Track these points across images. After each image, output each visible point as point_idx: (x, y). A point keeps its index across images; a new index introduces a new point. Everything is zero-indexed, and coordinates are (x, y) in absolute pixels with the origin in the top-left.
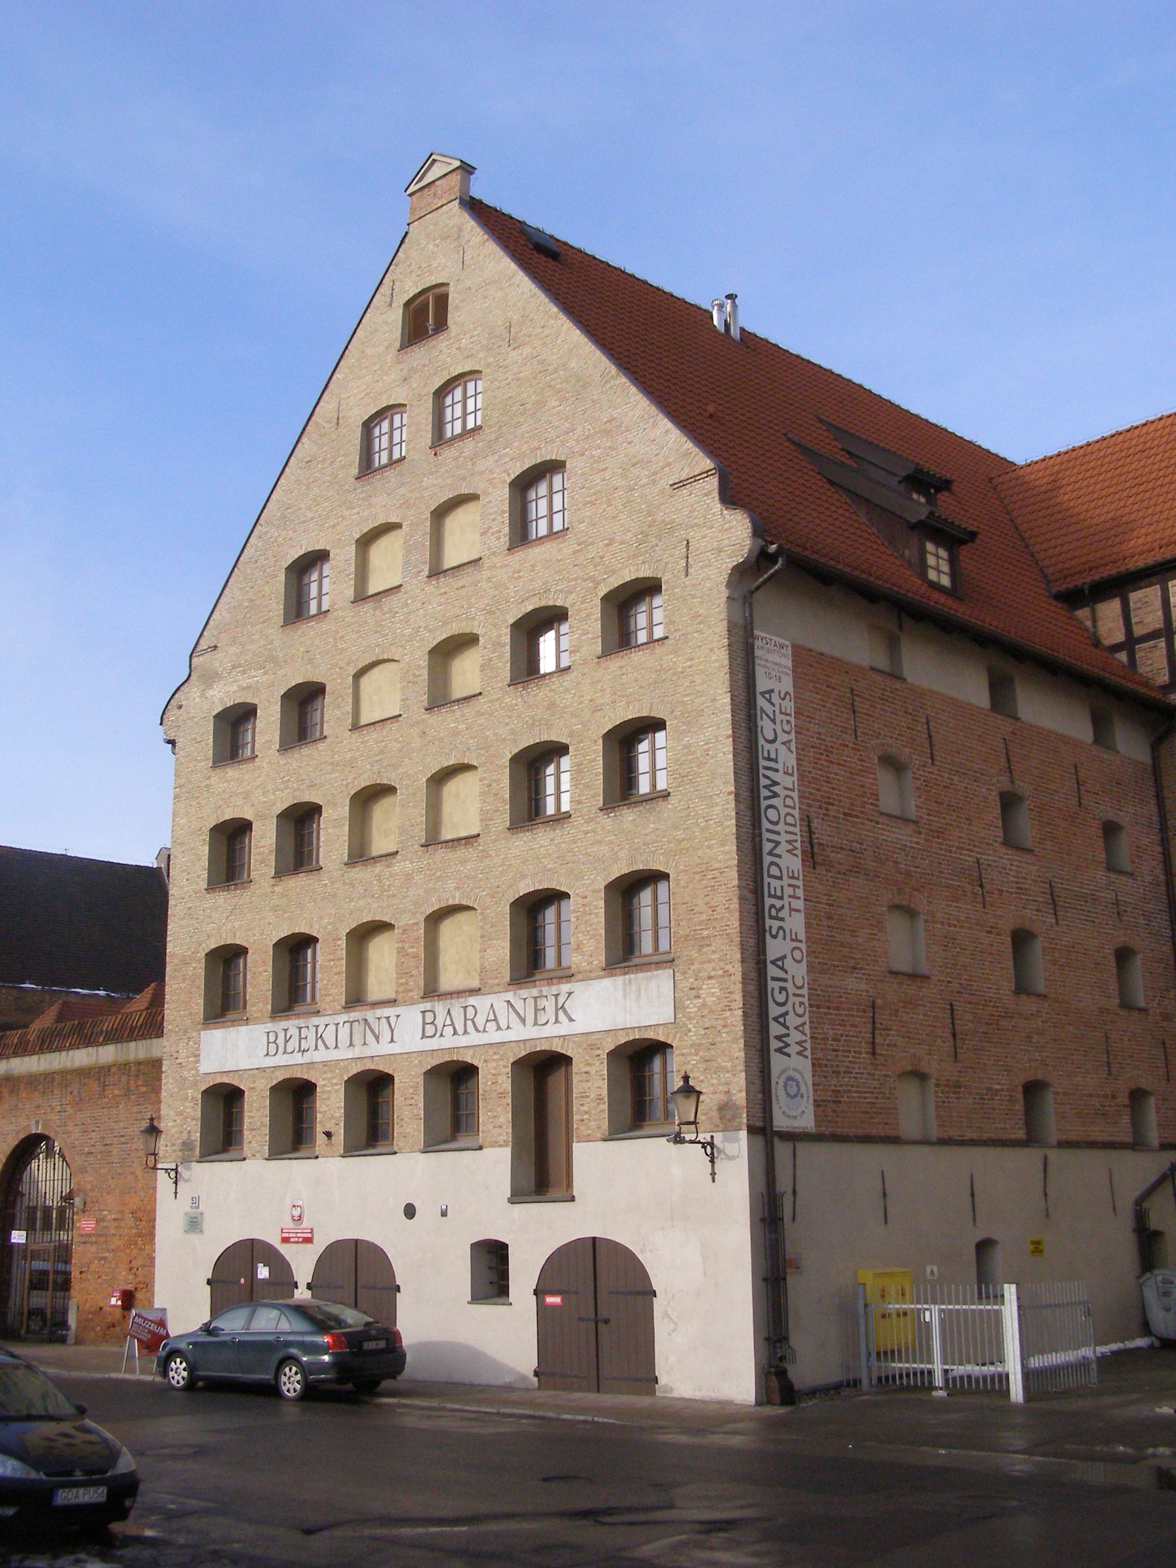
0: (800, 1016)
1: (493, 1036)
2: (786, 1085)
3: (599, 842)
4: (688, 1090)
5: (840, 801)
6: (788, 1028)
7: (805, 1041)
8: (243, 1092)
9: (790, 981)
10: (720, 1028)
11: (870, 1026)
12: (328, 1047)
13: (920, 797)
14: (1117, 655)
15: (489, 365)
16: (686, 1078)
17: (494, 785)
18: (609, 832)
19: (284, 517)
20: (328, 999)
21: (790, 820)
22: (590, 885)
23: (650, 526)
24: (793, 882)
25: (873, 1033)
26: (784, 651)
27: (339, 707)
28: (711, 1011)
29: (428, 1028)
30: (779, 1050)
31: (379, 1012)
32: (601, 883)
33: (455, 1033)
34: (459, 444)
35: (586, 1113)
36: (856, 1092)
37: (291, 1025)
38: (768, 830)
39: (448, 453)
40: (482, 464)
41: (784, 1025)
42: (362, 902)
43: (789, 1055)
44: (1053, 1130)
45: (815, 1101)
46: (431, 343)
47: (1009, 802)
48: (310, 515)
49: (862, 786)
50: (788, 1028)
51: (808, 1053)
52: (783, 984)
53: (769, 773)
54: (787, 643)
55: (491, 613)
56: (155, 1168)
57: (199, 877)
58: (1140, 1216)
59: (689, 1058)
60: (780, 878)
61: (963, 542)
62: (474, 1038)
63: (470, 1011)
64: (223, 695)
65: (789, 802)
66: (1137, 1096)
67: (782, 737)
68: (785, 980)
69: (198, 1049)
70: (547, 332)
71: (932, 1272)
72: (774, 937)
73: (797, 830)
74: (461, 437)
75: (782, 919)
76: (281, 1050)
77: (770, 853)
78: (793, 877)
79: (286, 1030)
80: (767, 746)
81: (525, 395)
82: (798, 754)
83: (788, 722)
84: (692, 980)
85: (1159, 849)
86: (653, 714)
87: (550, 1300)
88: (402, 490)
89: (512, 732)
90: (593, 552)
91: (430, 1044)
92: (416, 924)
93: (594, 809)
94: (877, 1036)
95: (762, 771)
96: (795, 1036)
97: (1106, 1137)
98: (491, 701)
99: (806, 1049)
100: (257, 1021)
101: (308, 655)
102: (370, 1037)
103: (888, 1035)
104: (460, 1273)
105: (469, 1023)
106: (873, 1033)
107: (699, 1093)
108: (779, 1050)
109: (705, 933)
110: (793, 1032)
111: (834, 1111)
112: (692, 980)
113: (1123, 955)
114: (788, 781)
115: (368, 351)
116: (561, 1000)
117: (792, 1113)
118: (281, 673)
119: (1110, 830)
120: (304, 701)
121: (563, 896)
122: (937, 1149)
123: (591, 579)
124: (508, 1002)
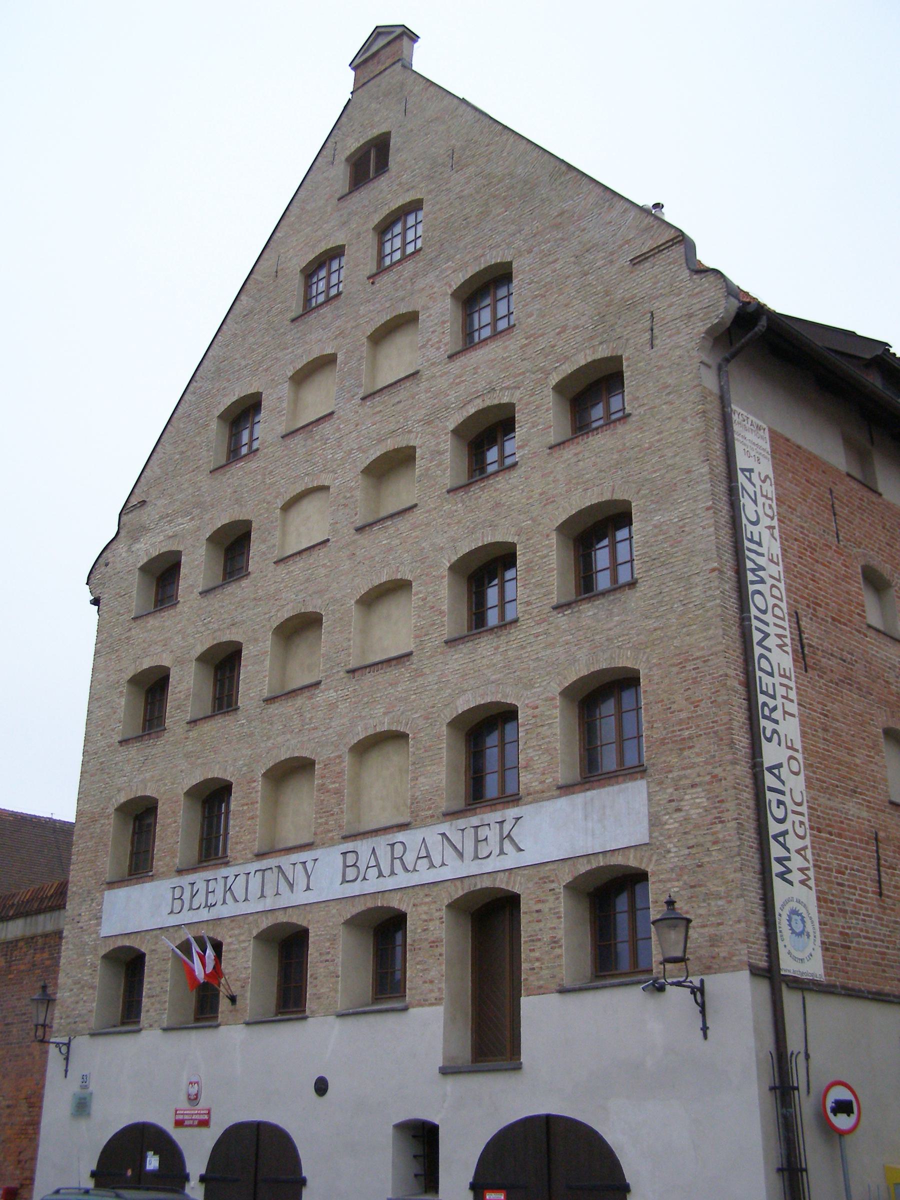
1: (426, 876)
2: (789, 921)
3: (552, 645)
4: (674, 919)
5: (827, 604)
6: (788, 850)
7: (808, 869)
8: (144, 955)
10: (709, 845)
11: (875, 861)
12: (242, 896)
16: (670, 903)
17: (430, 598)
18: (565, 631)
19: (219, 369)
20: (239, 847)
21: (777, 611)
24: (785, 681)
25: (879, 870)
27: (264, 541)
30: (781, 875)
32: (556, 688)
33: (381, 875)
35: (537, 960)
36: (865, 938)
38: (756, 618)
39: (385, 280)
40: (421, 283)
43: (791, 883)
45: (823, 943)
46: (372, 185)
48: (243, 363)
49: (847, 593)
50: (788, 850)
51: (812, 883)
52: (781, 797)
54: (765, 426)
55: (429, 423)
56: (43, 1041)
57: (113, 730)
59: (669, 885)
60: (771, 674)
62: (403, 880)
63: (399, 849)
64: (149, 547)
65: (775, 592)
67: (765, 521)
69: (101, 911)
72: (769, 740)
73: (786, 624)
75: (776, 722)
76: (187, 906)
77: (760, 643)
78: (784, 676)
80: (750, 528)
81: (468, 210)
82: (781, 543)
83: (770, 507)
84: (670, 790)
86: (615, 497)
88: (337, 323)
89: (454, 540)
90: (542, 343)
92: (340, 757)
93: (548, 609)
94: (883, 874)
96: (796, 862)
99: (809, 879)
100: (164, 876)
102: (283, 887)
103: (893, 875)
106: (879, 870)
107: (689, 921)
108: (781, 875)
109: (686, 733)
110: (794, 856)
111: (844, 959)
112: (670, 790)
114: (776, 570)
115: (308, 208)
116: (507, 827)
117: (799, 955)
118: (207, 517)
120: (233, 546)
123: (542, 370)
124: (443, 834)
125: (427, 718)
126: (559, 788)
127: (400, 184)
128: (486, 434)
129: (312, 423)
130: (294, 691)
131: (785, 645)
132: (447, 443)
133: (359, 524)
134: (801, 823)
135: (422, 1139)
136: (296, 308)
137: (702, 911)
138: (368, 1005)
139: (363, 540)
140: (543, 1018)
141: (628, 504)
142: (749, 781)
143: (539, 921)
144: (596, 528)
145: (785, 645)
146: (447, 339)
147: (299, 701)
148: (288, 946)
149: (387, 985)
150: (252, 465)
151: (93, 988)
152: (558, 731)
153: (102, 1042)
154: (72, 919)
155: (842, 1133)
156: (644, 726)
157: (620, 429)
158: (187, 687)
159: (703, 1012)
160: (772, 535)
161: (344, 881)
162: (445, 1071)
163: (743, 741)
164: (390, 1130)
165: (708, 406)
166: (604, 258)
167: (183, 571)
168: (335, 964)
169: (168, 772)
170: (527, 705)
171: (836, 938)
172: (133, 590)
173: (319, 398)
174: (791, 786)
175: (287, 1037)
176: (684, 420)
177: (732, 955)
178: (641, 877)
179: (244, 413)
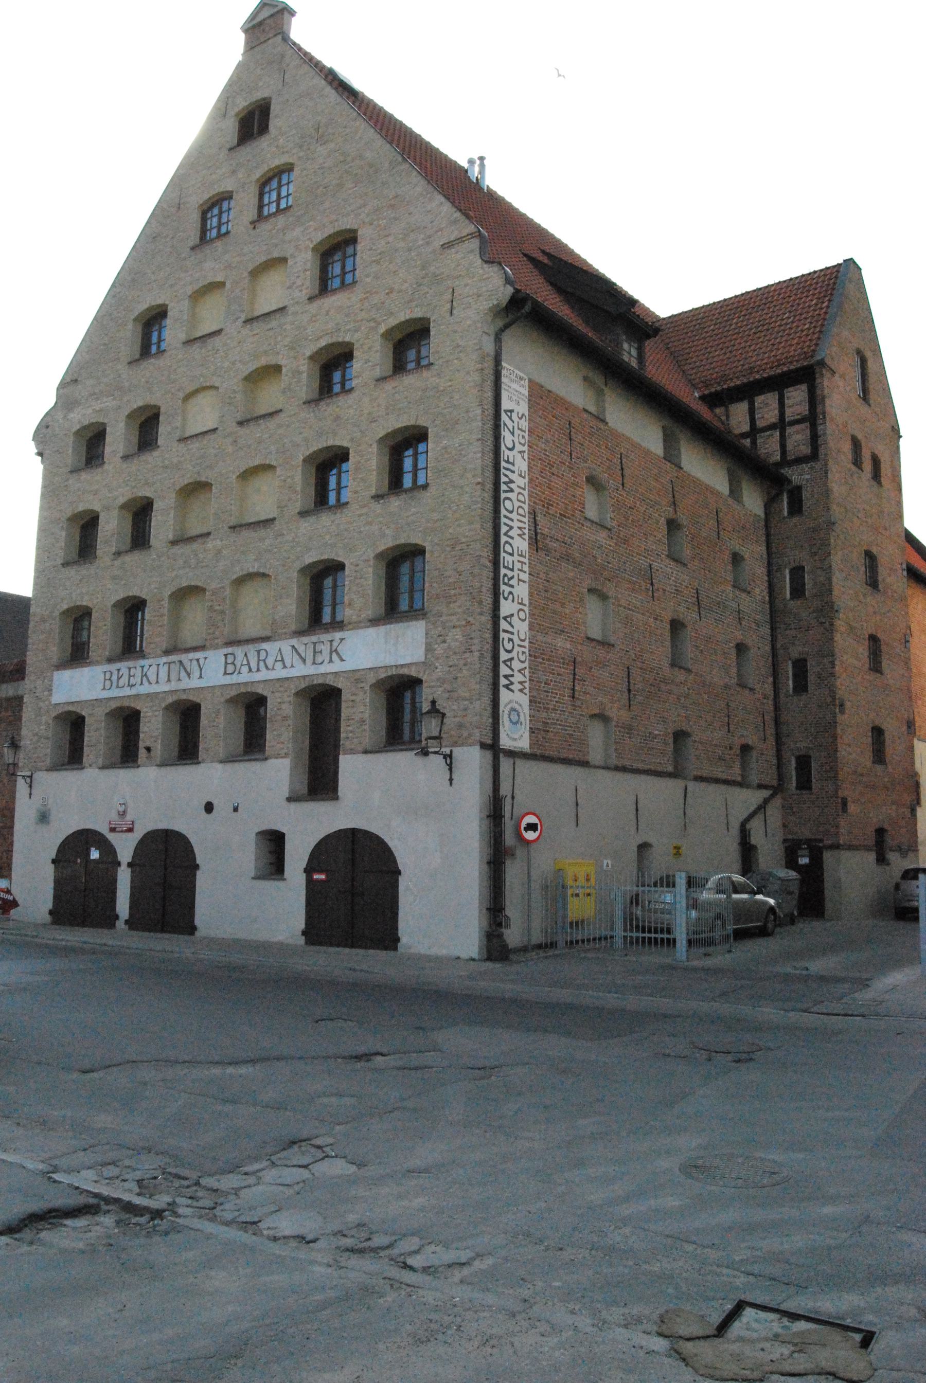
0: (522, 662)
1: (283, 674)
3: (370, 523)
4: (434, 710)
6: (513, 670)
9: (516, 633)
11: (572, 676)
12: (151, 681)
13: (613, 512)
14: (743, 441)
15: (300, 158)
16: (433, 702)
20: (153, 646)
21: (521, 511)
22: (362, 555)
23: (423, 278)
24: (522, 559)
26: (523, 382)
28: (455, 653)
29: (230, 666)
31: (192, 655)
33: (250, 670)
34: (272, 220)
35: (351, 732)
37: (123, 666)
38: (505, 517)
39: (265, 227)
41: (510, 668)
42: (181, 572)
43: (513, 691)
44: (693, 767)
47: (673, 525)
48: (153, 278)
49: (574, 496)
50: (513, 670)
51: (527, 691)
52: (511, 636)
53: (508, 473)
55: (292, 348)
56: (14, 774)
58: (744, 833)
59: (435, 689)
60: (512, 555)
61: (648, 337)
62: (264, 675)
64: (81, 417)
66: (746, 749)
67: (518, 447)
68: (512, 633)
69: (51, 686)
70: (348, 130)
71: (608, 865)
72: (506, 599)
74: (274, 214)
75: (512, 586)
76: (115, 684)
77: (506, 534)
78: (521, 555)
79: (119, 670)
80: (507, 452)
82: (529, 463)
83: (523, 437)
85: (766, 578)
87: (316, 877)
88: (227, 257)
89: (306, 440)
90: (375, 300)
91: (228, 680)
92: (223, 587)
95: (503, 471)
96: (518, 677)
97: (724, 776)
98: (290, 416)
99: (525, 688)
100: (98, 663)
101: (150, 385)
102: (183, 674)
104: (247, 855)
105: (262, 663)
106: (574, 682)
107: (444, 715)
108: (507, 687)
110: (516, 673)
111: (544, 738)
112: (440, 629)
113: (741, 648)
114: (522, 482)
116: (335, 644)
119: (736, 559)
120: (147, 426)
121: (340, 567)
122: (614, 773)
124: (293, 647)
125: (284, 566)
126: (370, 621)
127: (277, 147)
128: (333, 364)
129: (207, 335)
130: (191, 538)
131: (524, 534)
132: (304, 366)
133: (239, 419)
134: (523, 653)
135: (274, 842)
136: (194, 238)
137: (455, 707)
138: (240, 756)
139: (243, 431)
140: (351, 767)
141: (426, 429)
142: (489, 626)
143: (353, 707)
144: (405, 443)
145: (524, 534)
146: (308, 283)
147: (195, 546)
148: (187, 715)
149: (253, 743)
150: (161, 362)
151: (48, 738)
152: (371, 582)
153: (55, 775)
154: (29, 686)
155: (528, 842)
156: (427, 585)
157: (425, 374)
158: (112, 527)
159: (451, 770)
160: (523, 457)
161: (225, 673)
162: (289, 800)
163: (488, 600)
164: (252, 837)
165: (486, 365)
166: (423, 239)
167: (108, 439)
168: (218, 728)
169: (99, 589)
170: (352, 564)
171: (540, 725)
172: (70, 453)
173: (212, 315)
174: (518, 628)
175: (184, 774)
176: (468, 373)
177: (470, 735)
178: (419, 682)
179: (155, 318)
